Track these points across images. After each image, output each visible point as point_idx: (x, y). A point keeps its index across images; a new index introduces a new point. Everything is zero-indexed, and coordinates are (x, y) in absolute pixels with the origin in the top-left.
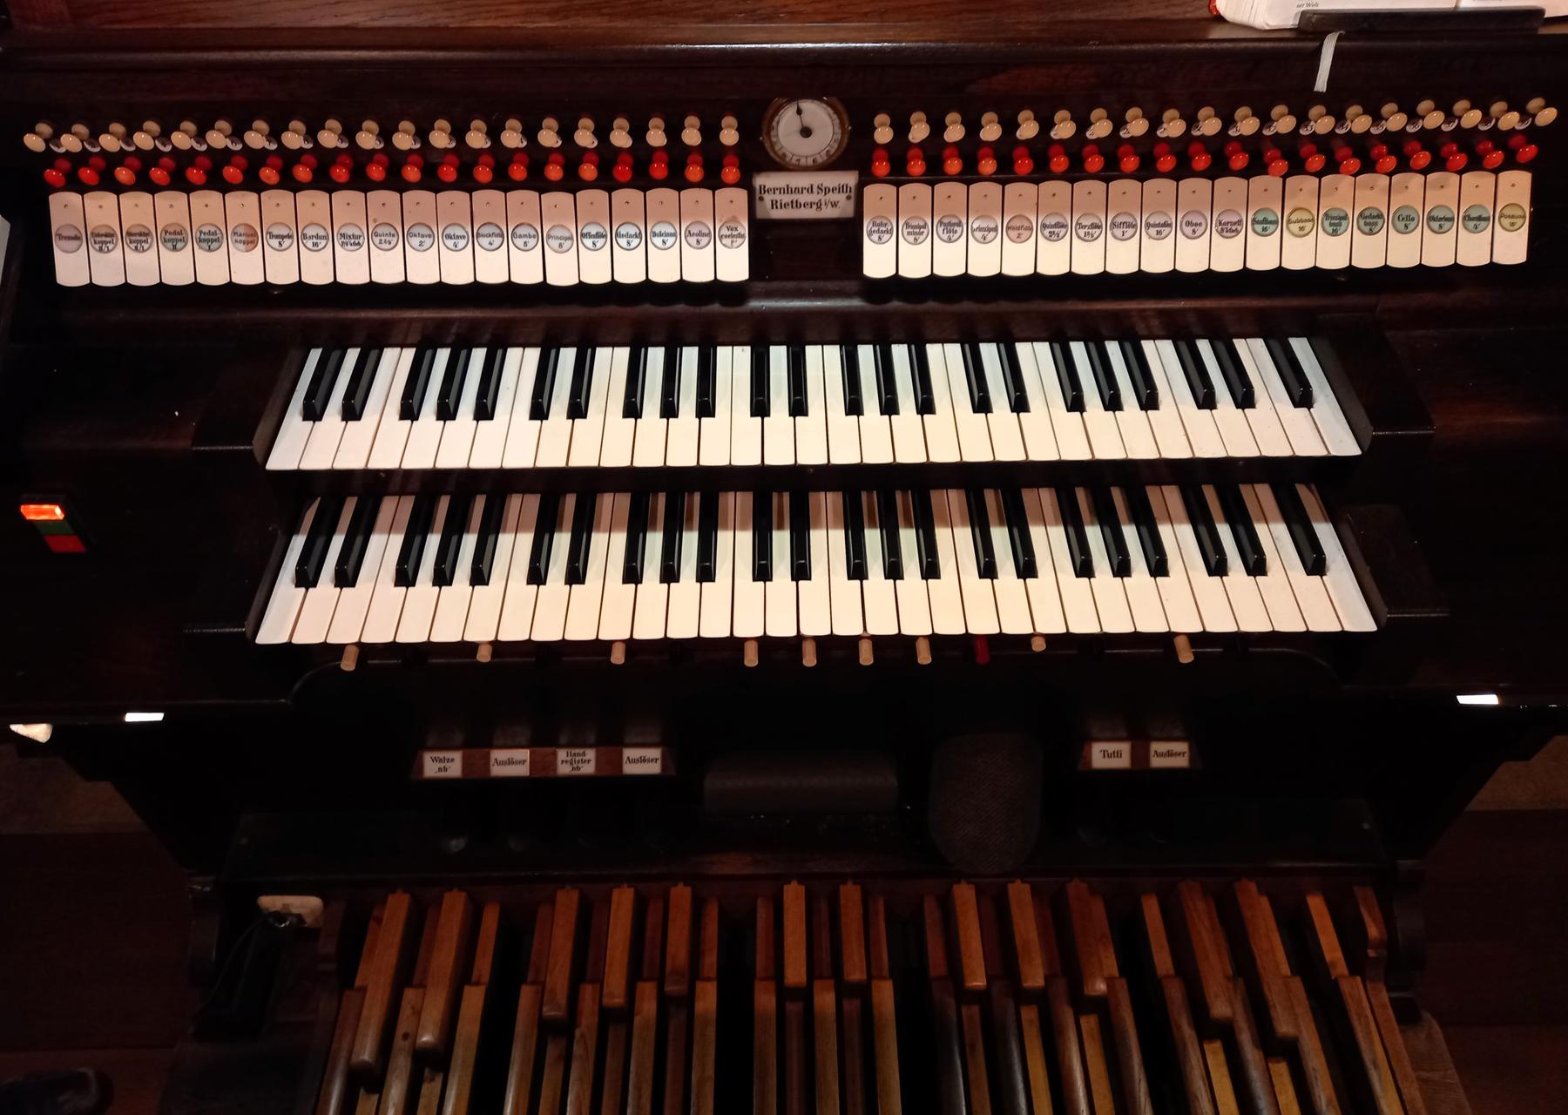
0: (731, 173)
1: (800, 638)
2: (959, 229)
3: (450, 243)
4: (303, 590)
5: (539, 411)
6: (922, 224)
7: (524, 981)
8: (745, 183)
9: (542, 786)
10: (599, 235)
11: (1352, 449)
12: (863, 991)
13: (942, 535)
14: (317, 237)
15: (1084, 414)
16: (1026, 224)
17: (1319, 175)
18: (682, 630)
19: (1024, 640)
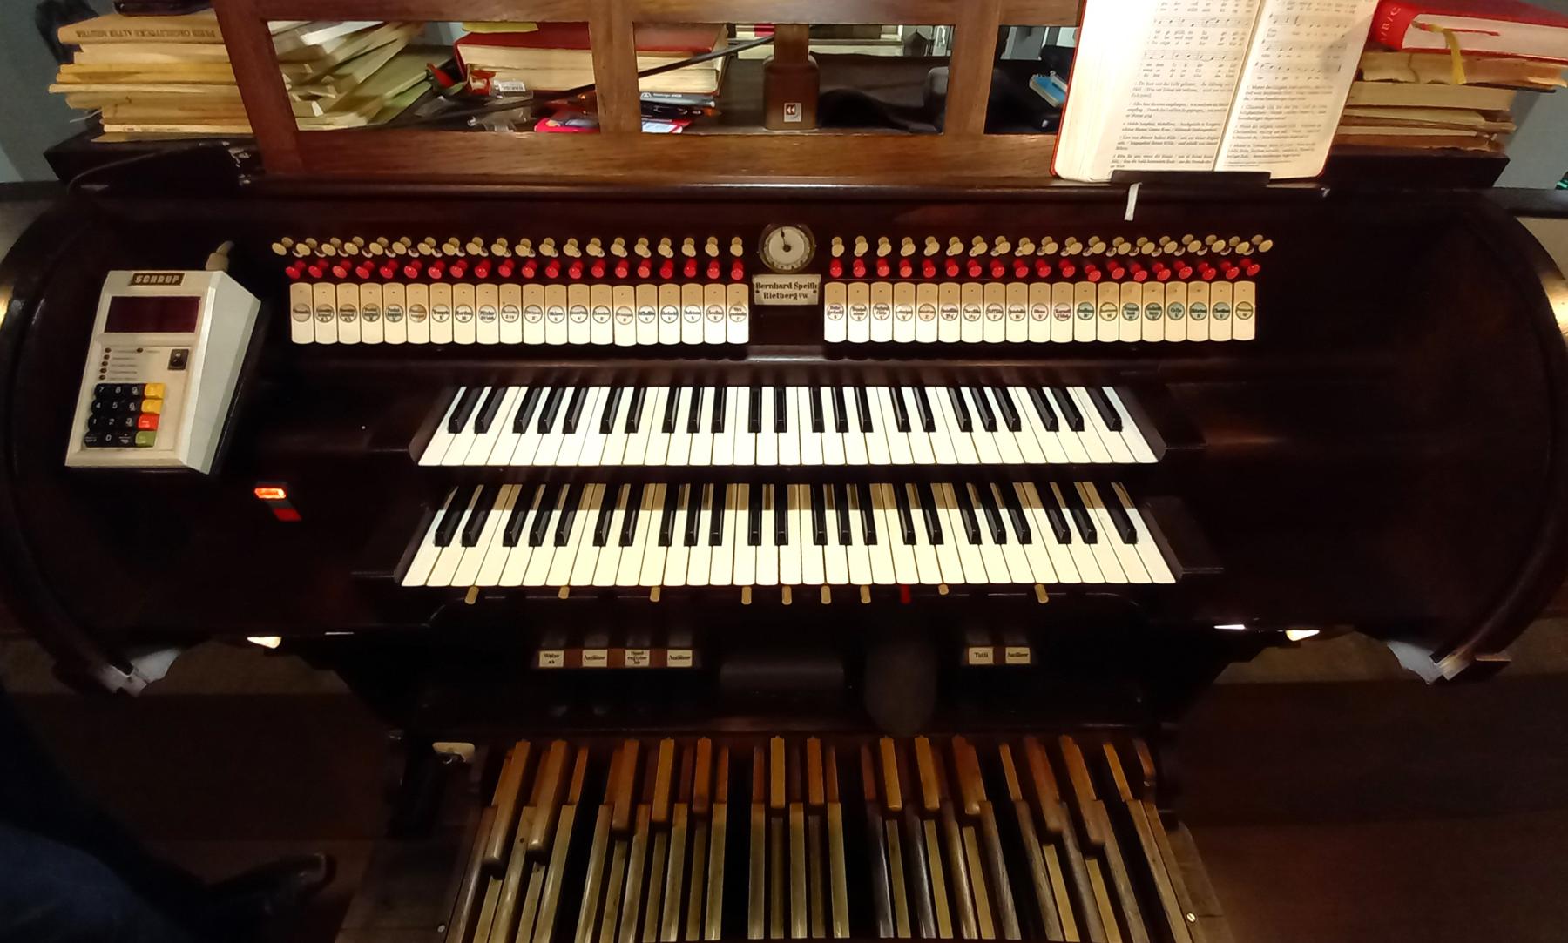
0: (737, 273)
1: (780, 586)
2: (887, 312)
3: (552, 318)
4: (440, 548)
5: (606, 428)
6: (863, 308)
7: (601, 802)
8: (747, 280)
9: (616, 675)
10: (650, 313)
11: (1151, 459)
12: (822, 811)
13: (878, 514)
14: (466, 313)
15: (972, 433)
16: (932, 310)
17: (1120, 281)
18: (698, 580)
19: (935, 587)
